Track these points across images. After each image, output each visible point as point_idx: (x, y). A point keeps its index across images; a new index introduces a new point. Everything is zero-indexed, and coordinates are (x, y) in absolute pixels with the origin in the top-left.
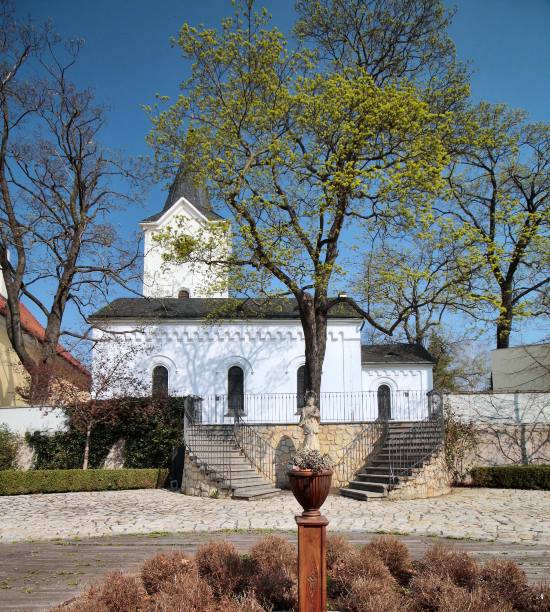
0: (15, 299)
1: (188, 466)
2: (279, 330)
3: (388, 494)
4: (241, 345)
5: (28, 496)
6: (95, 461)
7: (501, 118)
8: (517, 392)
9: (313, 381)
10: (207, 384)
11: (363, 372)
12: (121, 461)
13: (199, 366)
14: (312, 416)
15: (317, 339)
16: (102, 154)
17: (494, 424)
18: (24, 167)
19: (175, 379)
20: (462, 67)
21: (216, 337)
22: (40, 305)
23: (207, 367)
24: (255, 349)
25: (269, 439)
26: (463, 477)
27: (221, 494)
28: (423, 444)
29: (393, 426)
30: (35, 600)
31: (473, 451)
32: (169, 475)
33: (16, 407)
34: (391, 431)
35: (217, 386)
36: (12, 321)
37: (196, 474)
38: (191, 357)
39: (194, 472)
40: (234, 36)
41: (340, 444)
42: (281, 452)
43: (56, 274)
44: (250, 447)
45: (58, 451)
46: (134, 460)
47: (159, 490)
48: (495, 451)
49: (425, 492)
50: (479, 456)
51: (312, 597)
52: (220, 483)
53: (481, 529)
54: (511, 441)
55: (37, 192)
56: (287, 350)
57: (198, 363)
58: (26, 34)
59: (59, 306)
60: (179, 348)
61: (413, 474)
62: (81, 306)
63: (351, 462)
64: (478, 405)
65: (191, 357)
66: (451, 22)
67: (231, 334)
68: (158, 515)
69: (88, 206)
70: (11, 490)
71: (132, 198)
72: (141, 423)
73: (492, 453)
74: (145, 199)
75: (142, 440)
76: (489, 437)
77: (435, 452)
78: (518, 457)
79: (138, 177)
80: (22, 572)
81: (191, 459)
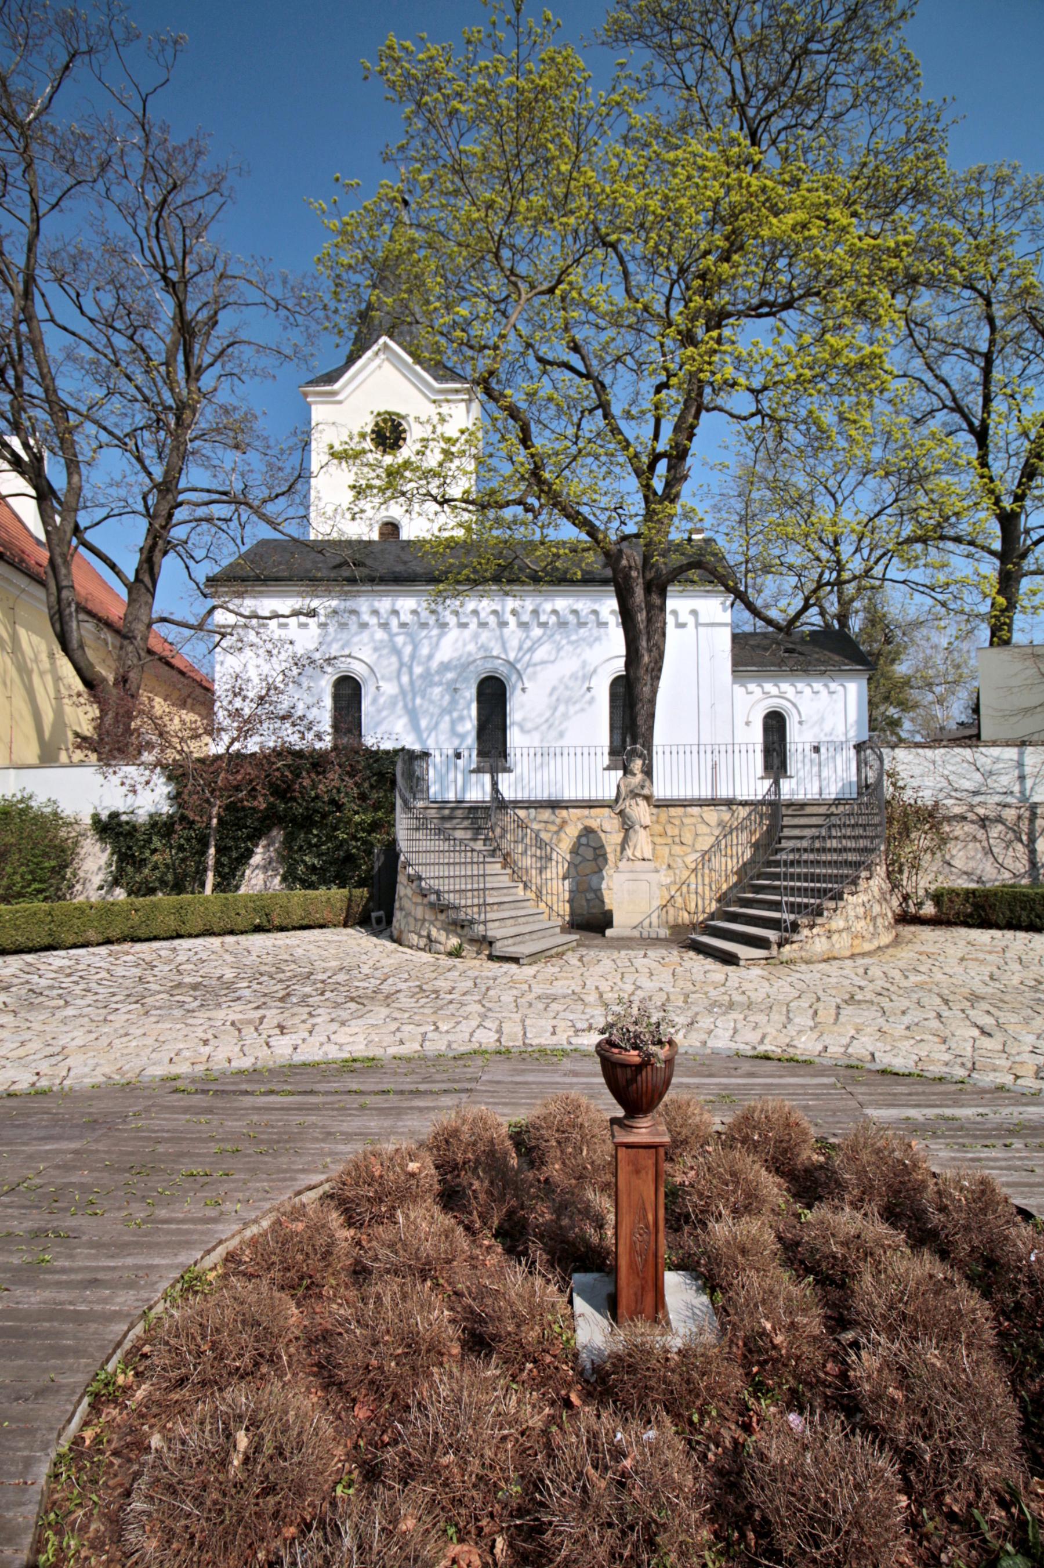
0: (64, 556)
1: (404, 890)
2: (575, 607)
3: (779, 953)
4: (502, 636)
5: (103, 950)
6: (227, 870)
7: (1008, 191)
8: (1023, 744)
9: (640, 721)
10: (437, 711)
11: (736, 687)
12: (275, 869)
13: (421, 676)
14: (639, 795)
15: (648, 640)
16: (226, 265)
17: (980, 804)
18: (74, 296)
19: (374, 701)
20: (933, 111)
21: (452, 620)
22: (113, 566)
23: (436, 679)
24: (528, 644)
25: (557, 833)
26: (920, 905)
27: (469, 950)
28: (845, 850)
29: (790, 812)
30: (150, 1246)
31: (938, 855)
32: (369, 900)
33: (71, 765)
34: (786, 821)
35: (455, 715)
36: (59, 600)
37: (420, 909)
38: (406, 659)
39: (416, 904)
40: (487, 68)
41: (690, 843)
42: (579, 859)
43: (141, 508)
44: (520, 848)
45: (154, 851)
46: (301, 868)
47: (350, 931)
48: (979, 856)
49: (847, 945)
50: (949, 864)
51: (640, 1267)
52: (466, 929)
53: (943, 1047)
54: (1011, 836)
55: (101, 343)
56: (591, 645)
57: (418, 670)
58: (68, 24)
59: (149, 566)
60: (381, 641)
61: (826, 913)
62: (191, 564)
63: (710, 877)
64: (950, 768)
65: (406, 659)
66: (913, 15)
67: (483, 615)
68: (352, 1005)
69: (200, 370)
70: (71, 939)
71: (288, 351)
72: (313, 800)
73: (973, 858)
74: (312, 355)
75: (315, 832)
76: (969, 828)
77: (869, 868)
78: (1022, 866)
79: (298, 309)
80: (119, 1170)
81: (411, 879)
